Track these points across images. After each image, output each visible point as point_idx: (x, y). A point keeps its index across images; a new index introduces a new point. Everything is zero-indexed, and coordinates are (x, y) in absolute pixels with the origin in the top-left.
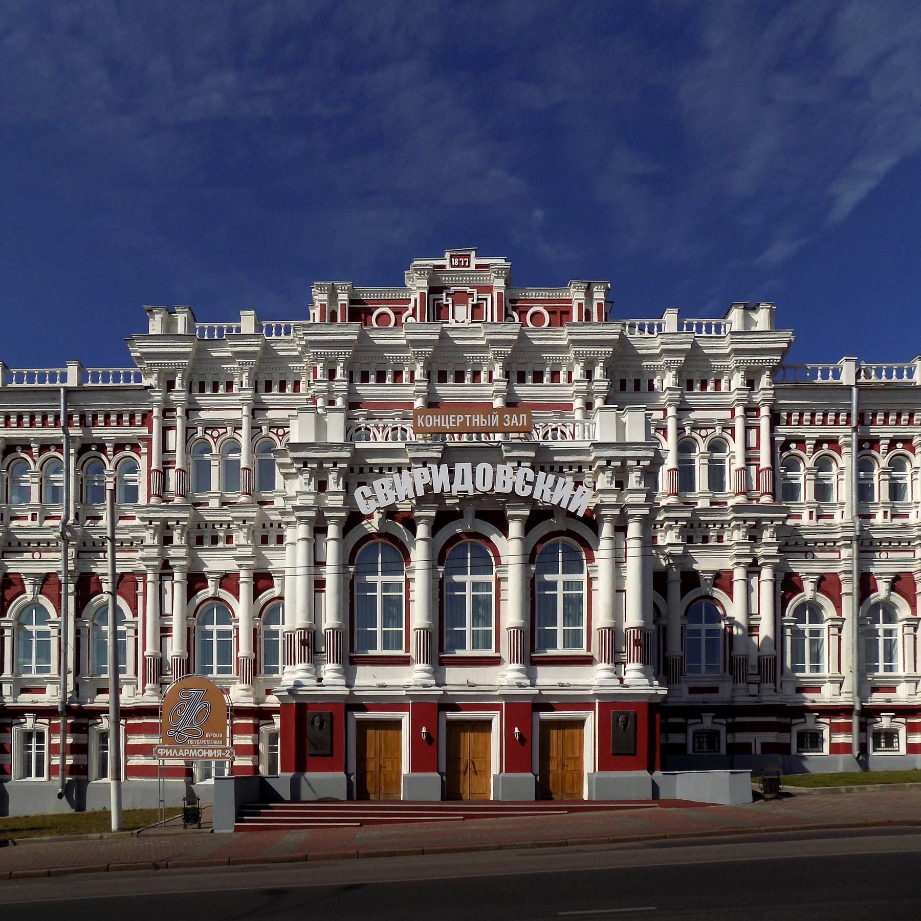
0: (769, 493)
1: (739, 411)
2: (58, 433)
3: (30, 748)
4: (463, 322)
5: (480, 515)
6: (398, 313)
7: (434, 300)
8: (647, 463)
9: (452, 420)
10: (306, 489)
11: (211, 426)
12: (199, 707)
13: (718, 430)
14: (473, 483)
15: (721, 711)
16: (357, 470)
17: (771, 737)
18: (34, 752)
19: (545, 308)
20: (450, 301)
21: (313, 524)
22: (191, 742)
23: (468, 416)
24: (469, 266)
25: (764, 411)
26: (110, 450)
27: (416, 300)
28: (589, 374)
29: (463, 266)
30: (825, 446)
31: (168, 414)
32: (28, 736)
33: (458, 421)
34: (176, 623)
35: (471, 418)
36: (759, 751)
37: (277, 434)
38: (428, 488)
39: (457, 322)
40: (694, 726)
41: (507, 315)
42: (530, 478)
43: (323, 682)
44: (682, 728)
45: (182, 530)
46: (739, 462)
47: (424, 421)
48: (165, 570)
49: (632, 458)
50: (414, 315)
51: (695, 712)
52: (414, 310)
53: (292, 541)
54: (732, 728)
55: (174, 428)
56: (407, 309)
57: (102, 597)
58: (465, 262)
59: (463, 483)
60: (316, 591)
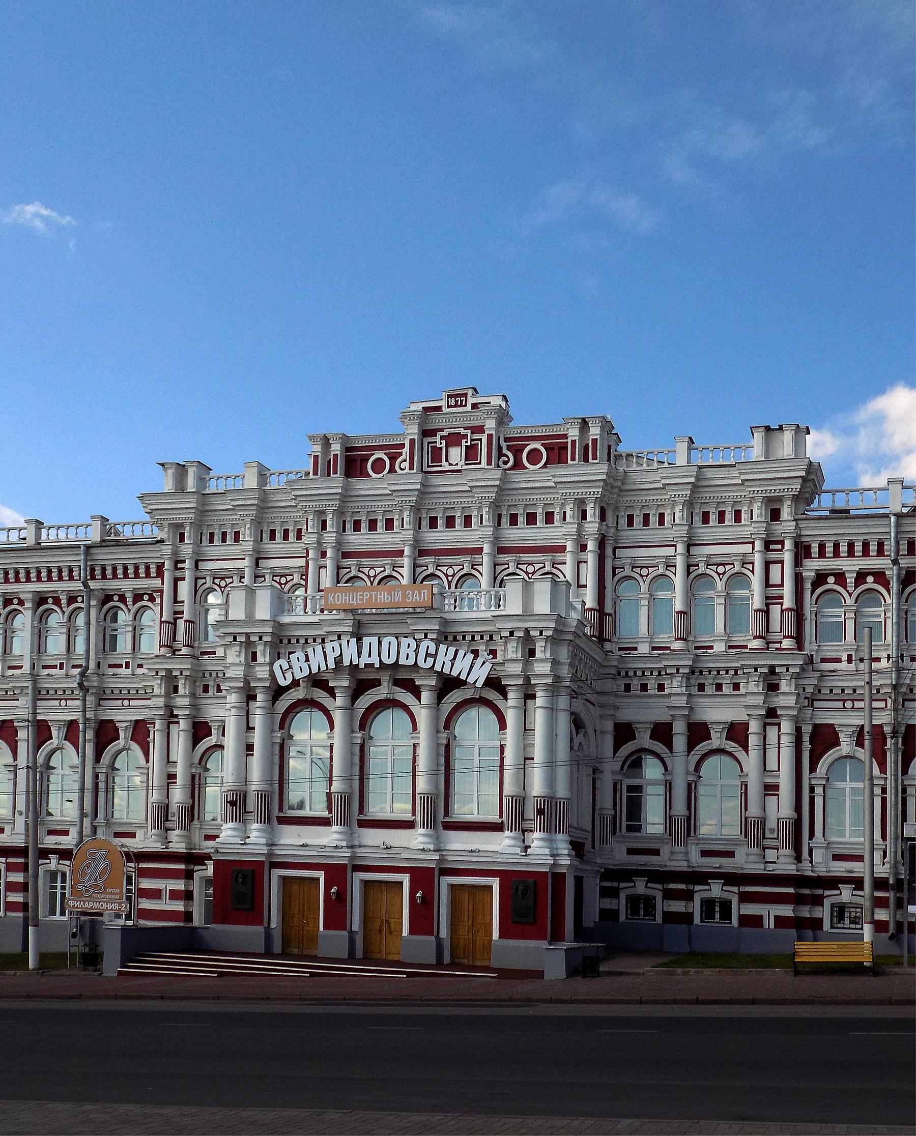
0: (791, 637)
1: (758, 545)
2: (78, 586)
3: (56, 888)
4: (457, 464)
5: (397, 683)
7: (429, 443)
8: (550, 633)
11: (218, 576)
12: (102, 865)
13: (737, 568)
14: (379, 655)
15: (731, 879)
17: (787, 911)
18: (59, 891)
20: (444, 445)
22: (95, 895)
24: (466, 405)
25: (788, 544)
26: (129, 600)
29: (460, 406)
30: (870, 579)
31: (180, 566)
32: (53, 875)
34: (180, 770)
36: (772, 926)
38: (339, 661)
39: (450, 464)
40: (701, 892)
41: (500, 454)
42: (432, 650)
44: (688, 896)
45: (186, 680)
46: (757, 602)
47: (334, 598)
48: (171, 717)
49: (535, 629)
51: (703, 878)
54: (745, 898)
55: (183, 579)
57: (119, 744)
58: (462, 401)
59: (370, 656)
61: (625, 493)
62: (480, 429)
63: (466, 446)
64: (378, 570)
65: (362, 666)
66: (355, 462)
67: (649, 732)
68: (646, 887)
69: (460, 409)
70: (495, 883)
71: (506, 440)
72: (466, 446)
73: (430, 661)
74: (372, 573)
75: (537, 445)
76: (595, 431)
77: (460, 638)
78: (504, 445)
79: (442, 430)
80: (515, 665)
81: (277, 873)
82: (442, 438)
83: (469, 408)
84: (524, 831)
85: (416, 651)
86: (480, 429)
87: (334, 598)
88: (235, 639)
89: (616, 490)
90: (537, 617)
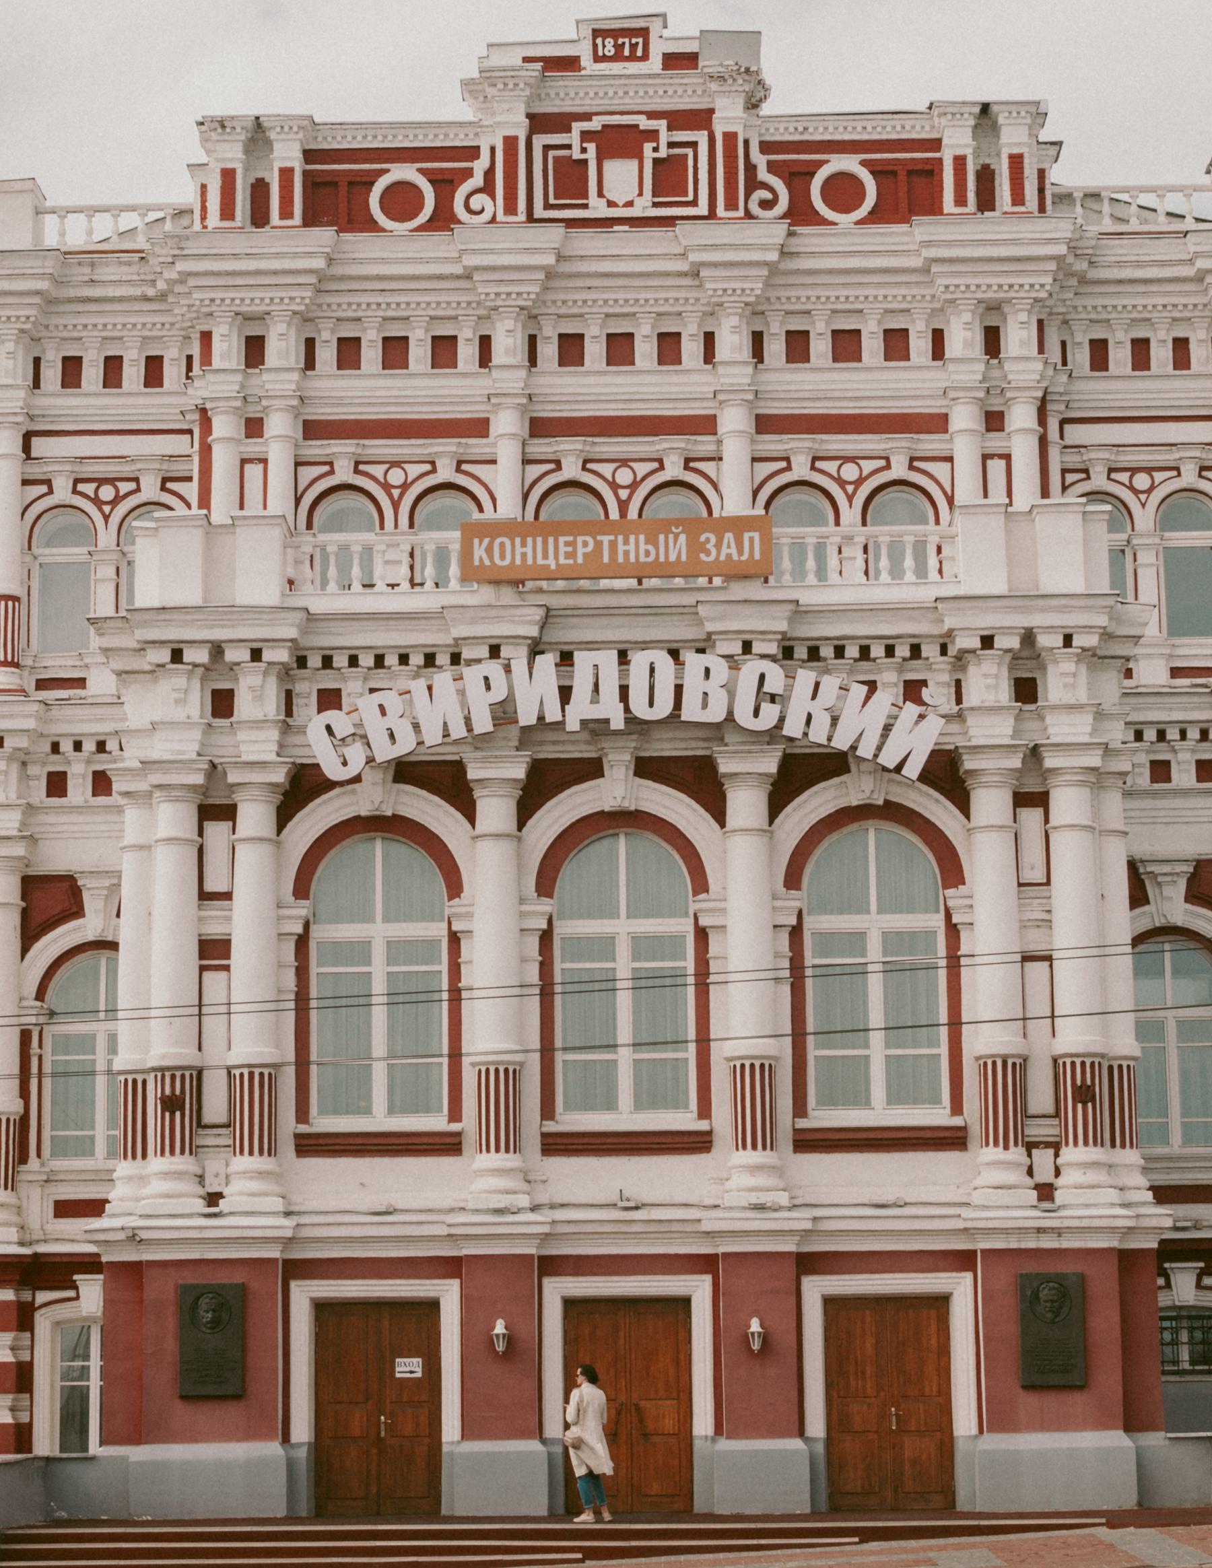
4: (630, 204)
5: (646, 768)
6: (445, 184)
9: (562, 549)
10: (179, 714)
16: (315, 661)
19: (864, 163)
21: (198, 799)
23: (606, 539)
27: (493, 149)
28: (992, 341)
33: (581, 551)
35: (613, 546)
37: (97, 501)
38: (504, 713)
39: (611, 204)
41: (753, 184)
42: (776, 682)
43: (223, 1205)
47: (489, 550)
49: (1050, 629)
50: (488, 188)
52: (489, 174)
53: (141, 841)
56: (469, 173)
58: (634, 47)
60: (203, 969)
61: (1090, 289)
62: (701, 119)
63: (656, 161)
64: (414, 470)
65: (573, 725)
66: (337, 187)
67: (1182, 884)
68: (1199, 1286)
69: (633, 68)
70: (962, 1290)
71: (766, 147)
72: (656, 161)
73: (770, 713)
74: (396, 477)
75: (849, 163)
76: (1013, 137)
77: (827, 651)
78: (760, 160)
79: (587, 117)
80: (995, 719)
81: (303, 1294)
82: (586, 136)
83: (655, 63)
84: (1030, 1147)
85: (730, 690)
86: (701, 119)
87: (489, 550)
88: (177, 656)
89: (1074, 282)
90: (1054, 602)
